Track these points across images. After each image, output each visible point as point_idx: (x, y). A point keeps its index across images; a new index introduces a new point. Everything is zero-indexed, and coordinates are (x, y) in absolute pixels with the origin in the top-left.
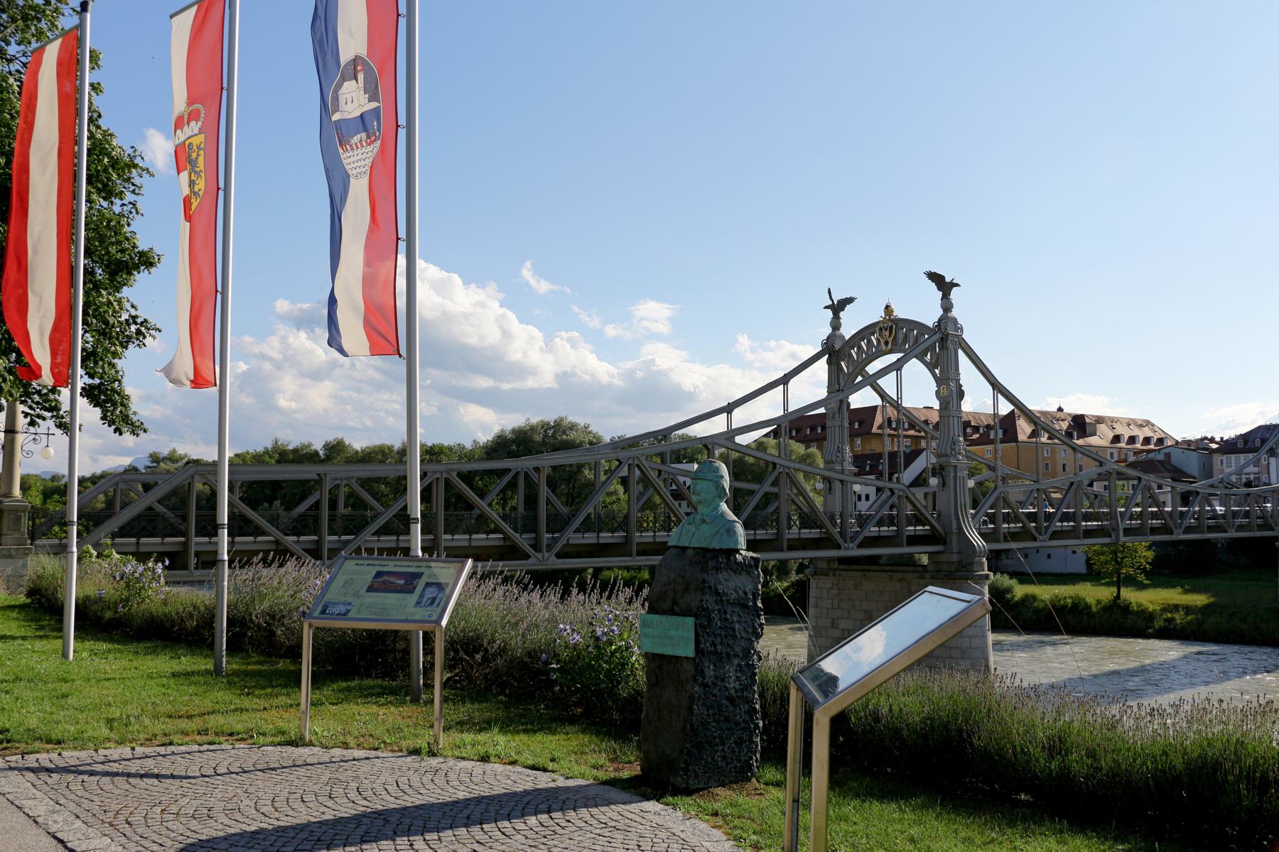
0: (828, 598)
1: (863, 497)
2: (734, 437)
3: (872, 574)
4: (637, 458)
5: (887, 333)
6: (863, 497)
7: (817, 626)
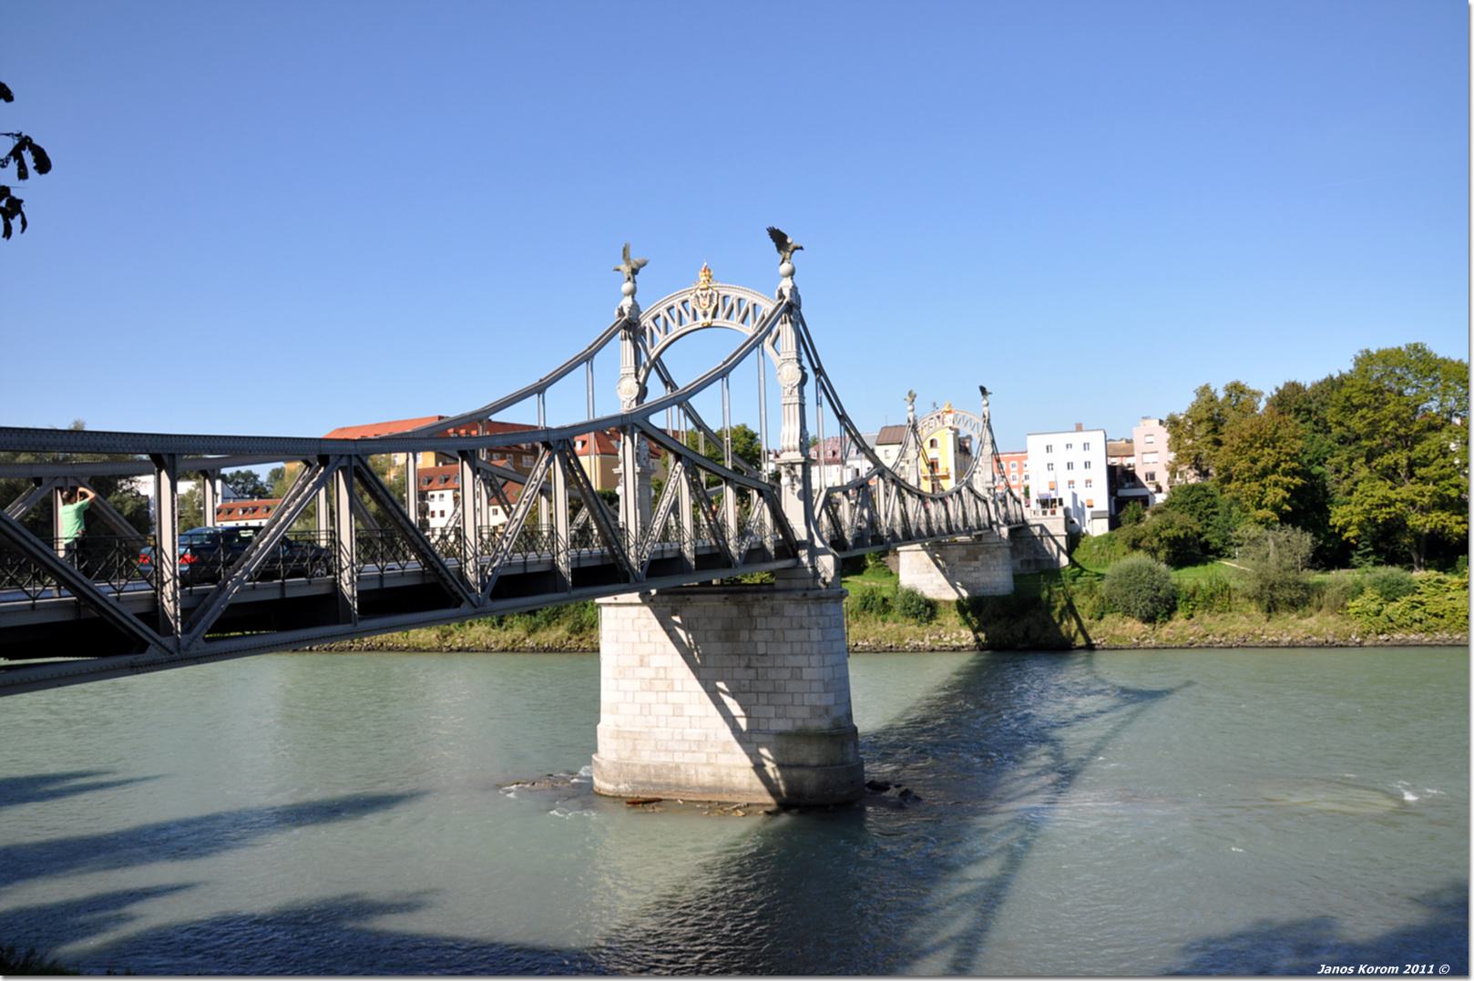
0: (634, 630)
1: (438, 514)
2: (648, 416)
3: (698, 597)
4: (357, 456)
5: (707, 302)
6: (438, 514)
7: (618, 666)
